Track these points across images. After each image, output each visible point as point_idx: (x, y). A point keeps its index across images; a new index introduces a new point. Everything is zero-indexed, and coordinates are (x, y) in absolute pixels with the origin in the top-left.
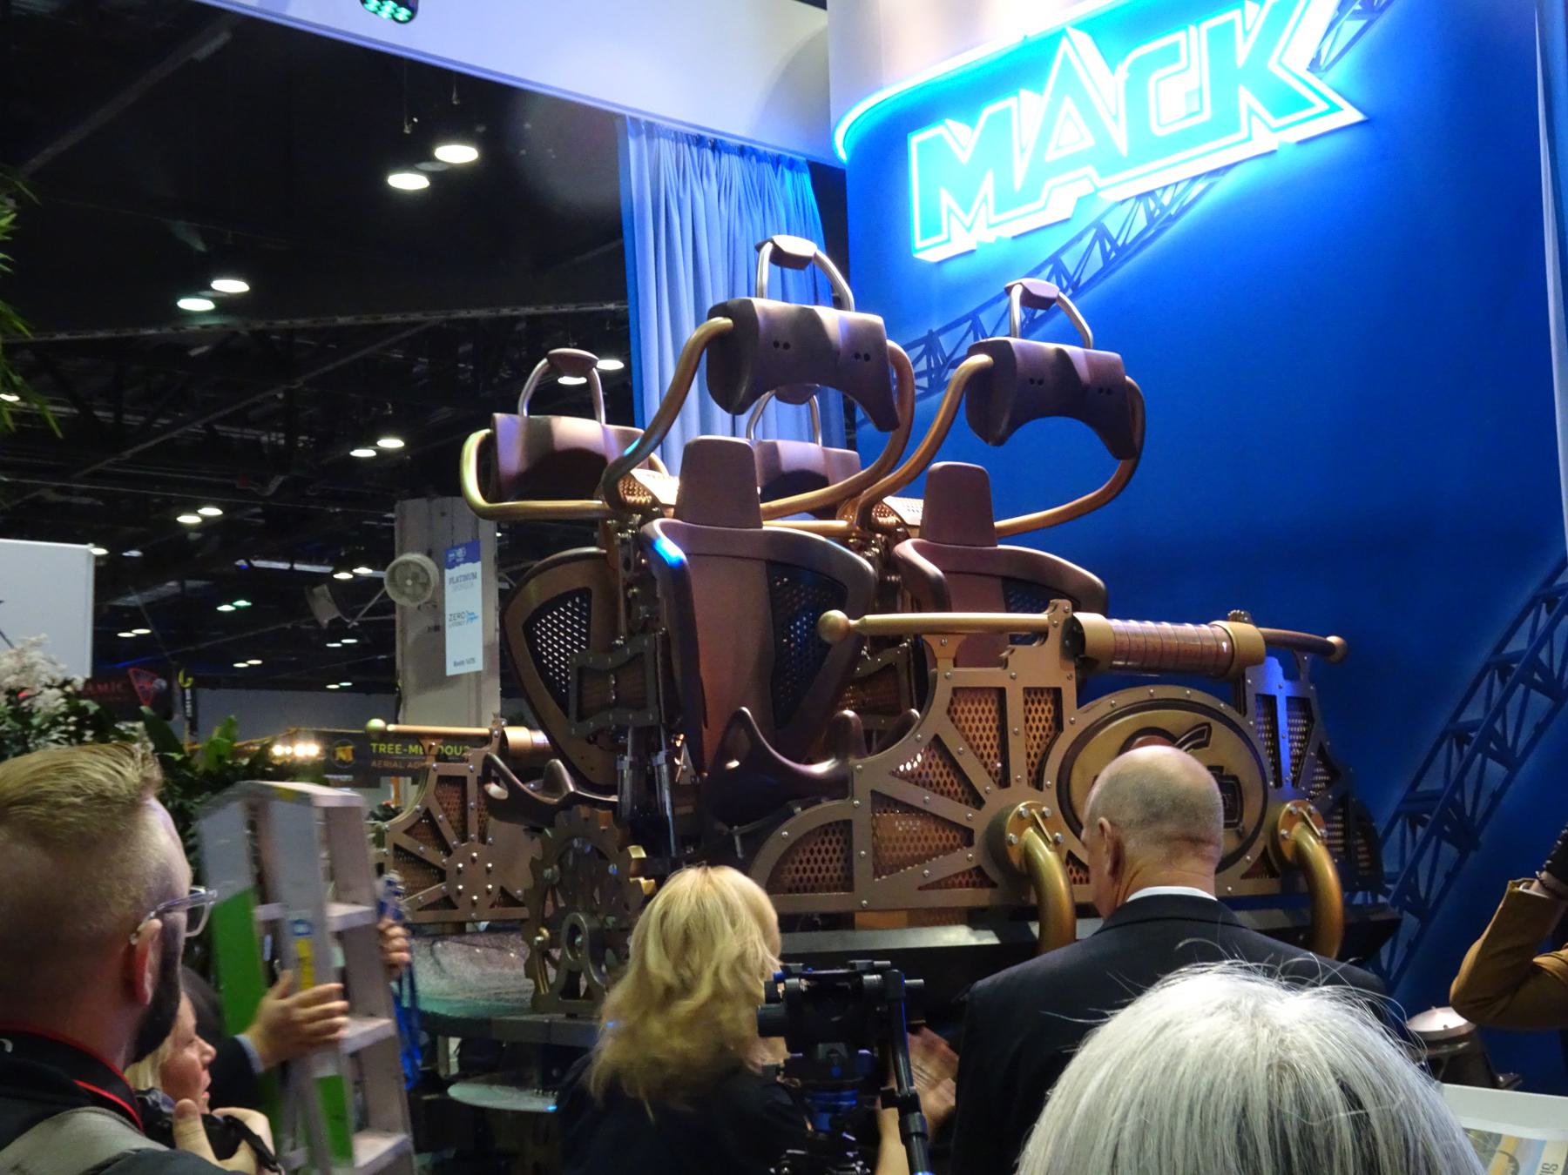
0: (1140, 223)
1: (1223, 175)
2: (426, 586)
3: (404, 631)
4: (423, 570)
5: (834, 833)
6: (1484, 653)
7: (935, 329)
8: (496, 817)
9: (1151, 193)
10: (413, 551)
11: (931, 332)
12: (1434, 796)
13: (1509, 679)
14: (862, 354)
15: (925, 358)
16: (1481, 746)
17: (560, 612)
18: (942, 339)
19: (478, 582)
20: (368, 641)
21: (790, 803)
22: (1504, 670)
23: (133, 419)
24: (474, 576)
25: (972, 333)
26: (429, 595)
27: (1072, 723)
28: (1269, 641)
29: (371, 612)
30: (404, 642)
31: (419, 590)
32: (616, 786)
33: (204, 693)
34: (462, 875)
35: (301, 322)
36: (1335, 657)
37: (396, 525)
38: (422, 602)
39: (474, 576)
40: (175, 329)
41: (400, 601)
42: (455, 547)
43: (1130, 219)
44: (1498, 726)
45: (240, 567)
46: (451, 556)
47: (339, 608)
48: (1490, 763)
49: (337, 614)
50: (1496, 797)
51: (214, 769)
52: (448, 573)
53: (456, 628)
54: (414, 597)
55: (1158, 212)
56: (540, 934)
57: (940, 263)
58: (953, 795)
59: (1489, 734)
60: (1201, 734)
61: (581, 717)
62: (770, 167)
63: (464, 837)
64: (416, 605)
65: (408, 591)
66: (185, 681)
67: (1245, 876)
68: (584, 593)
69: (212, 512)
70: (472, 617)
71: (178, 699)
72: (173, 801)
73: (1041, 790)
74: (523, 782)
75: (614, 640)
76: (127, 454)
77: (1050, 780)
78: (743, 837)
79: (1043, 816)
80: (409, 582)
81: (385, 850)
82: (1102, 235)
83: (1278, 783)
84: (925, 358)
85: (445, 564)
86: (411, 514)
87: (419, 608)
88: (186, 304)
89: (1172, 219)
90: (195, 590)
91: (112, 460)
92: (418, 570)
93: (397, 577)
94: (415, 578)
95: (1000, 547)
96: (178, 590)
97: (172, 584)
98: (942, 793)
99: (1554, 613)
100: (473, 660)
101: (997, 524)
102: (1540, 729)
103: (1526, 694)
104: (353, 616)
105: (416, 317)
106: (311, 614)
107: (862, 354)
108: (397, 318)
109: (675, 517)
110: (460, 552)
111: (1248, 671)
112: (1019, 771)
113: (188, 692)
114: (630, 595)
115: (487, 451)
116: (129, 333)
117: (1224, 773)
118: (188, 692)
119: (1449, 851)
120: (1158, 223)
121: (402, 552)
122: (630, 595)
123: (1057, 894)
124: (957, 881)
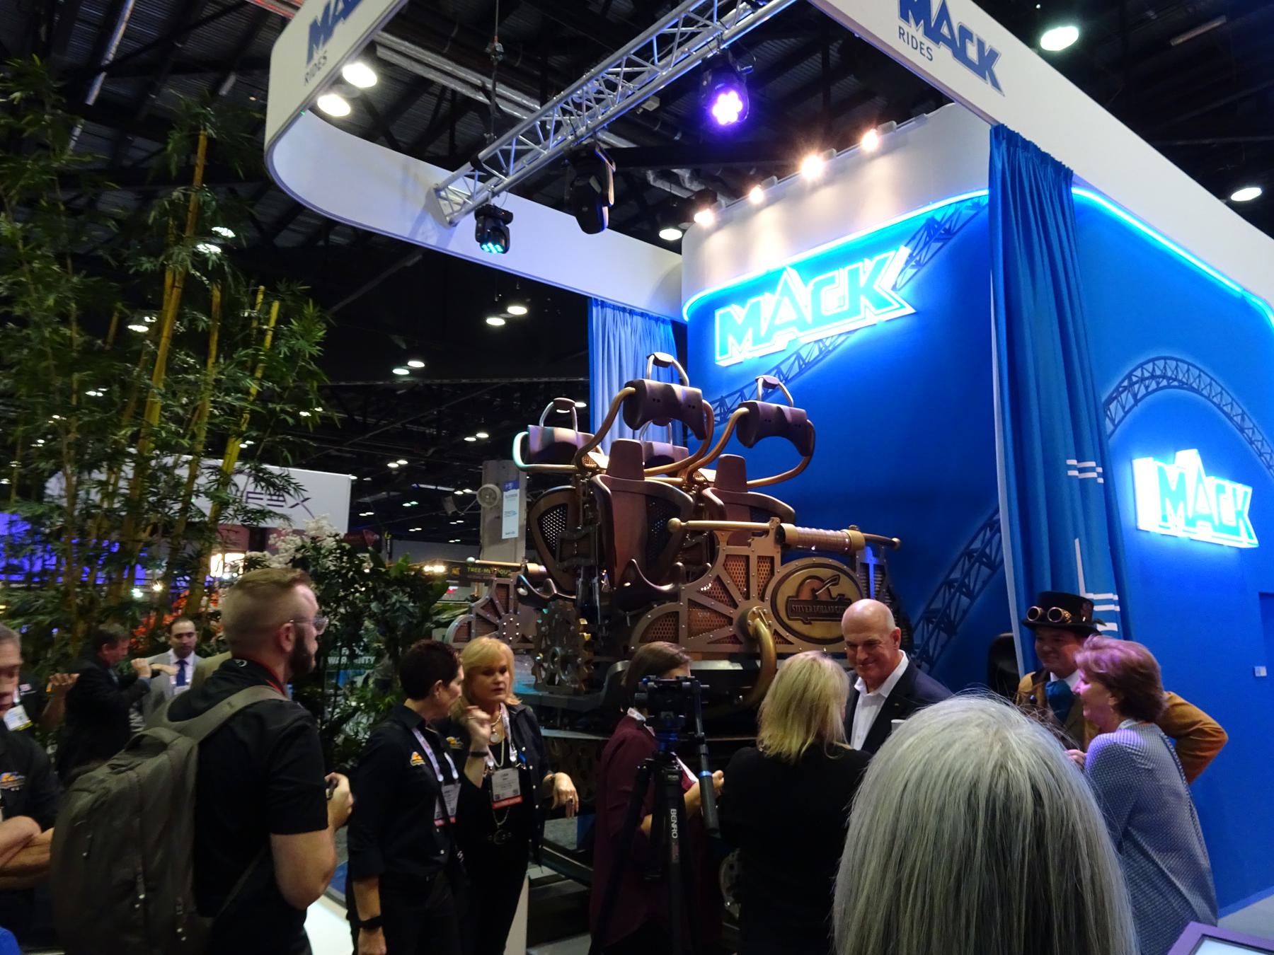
0: (816, 353)
2: (495, 499)
3: (484, 517)
4: (494, 492)
6: (962, 548)
7: (724, 395)
10: (490, 483)
18: (727, 400)
23: (371, 420)
24: (516, 495)
31: (492, 500)
33: (395, 542)
37: (483, 471)
39: (516, 495)
41: (483, 505)
54: (489, 503)
59: (962, 584)
60: (835, 580)
61: (561, 560)
70: (515, 513)
71: (384, 544)
76: (367, 436)
77: (768, 597)
79: (764, 613)
82: (799, 357)
85: (504, 489)
89: (830, 352)
90: (394, 496)
94: (490, 495)
97: (384, 493)
101: (748, 482)
103: (979, 567)
104: (462, 510)
106: (444, 509)
108: (488, 381)
109: (606, 474)
110: (510, 485)
112: (754, 593)
115: (525, 441)
116: (371, 383)
119: (943, 636)
120: (824, 353)
121: (485, 483)
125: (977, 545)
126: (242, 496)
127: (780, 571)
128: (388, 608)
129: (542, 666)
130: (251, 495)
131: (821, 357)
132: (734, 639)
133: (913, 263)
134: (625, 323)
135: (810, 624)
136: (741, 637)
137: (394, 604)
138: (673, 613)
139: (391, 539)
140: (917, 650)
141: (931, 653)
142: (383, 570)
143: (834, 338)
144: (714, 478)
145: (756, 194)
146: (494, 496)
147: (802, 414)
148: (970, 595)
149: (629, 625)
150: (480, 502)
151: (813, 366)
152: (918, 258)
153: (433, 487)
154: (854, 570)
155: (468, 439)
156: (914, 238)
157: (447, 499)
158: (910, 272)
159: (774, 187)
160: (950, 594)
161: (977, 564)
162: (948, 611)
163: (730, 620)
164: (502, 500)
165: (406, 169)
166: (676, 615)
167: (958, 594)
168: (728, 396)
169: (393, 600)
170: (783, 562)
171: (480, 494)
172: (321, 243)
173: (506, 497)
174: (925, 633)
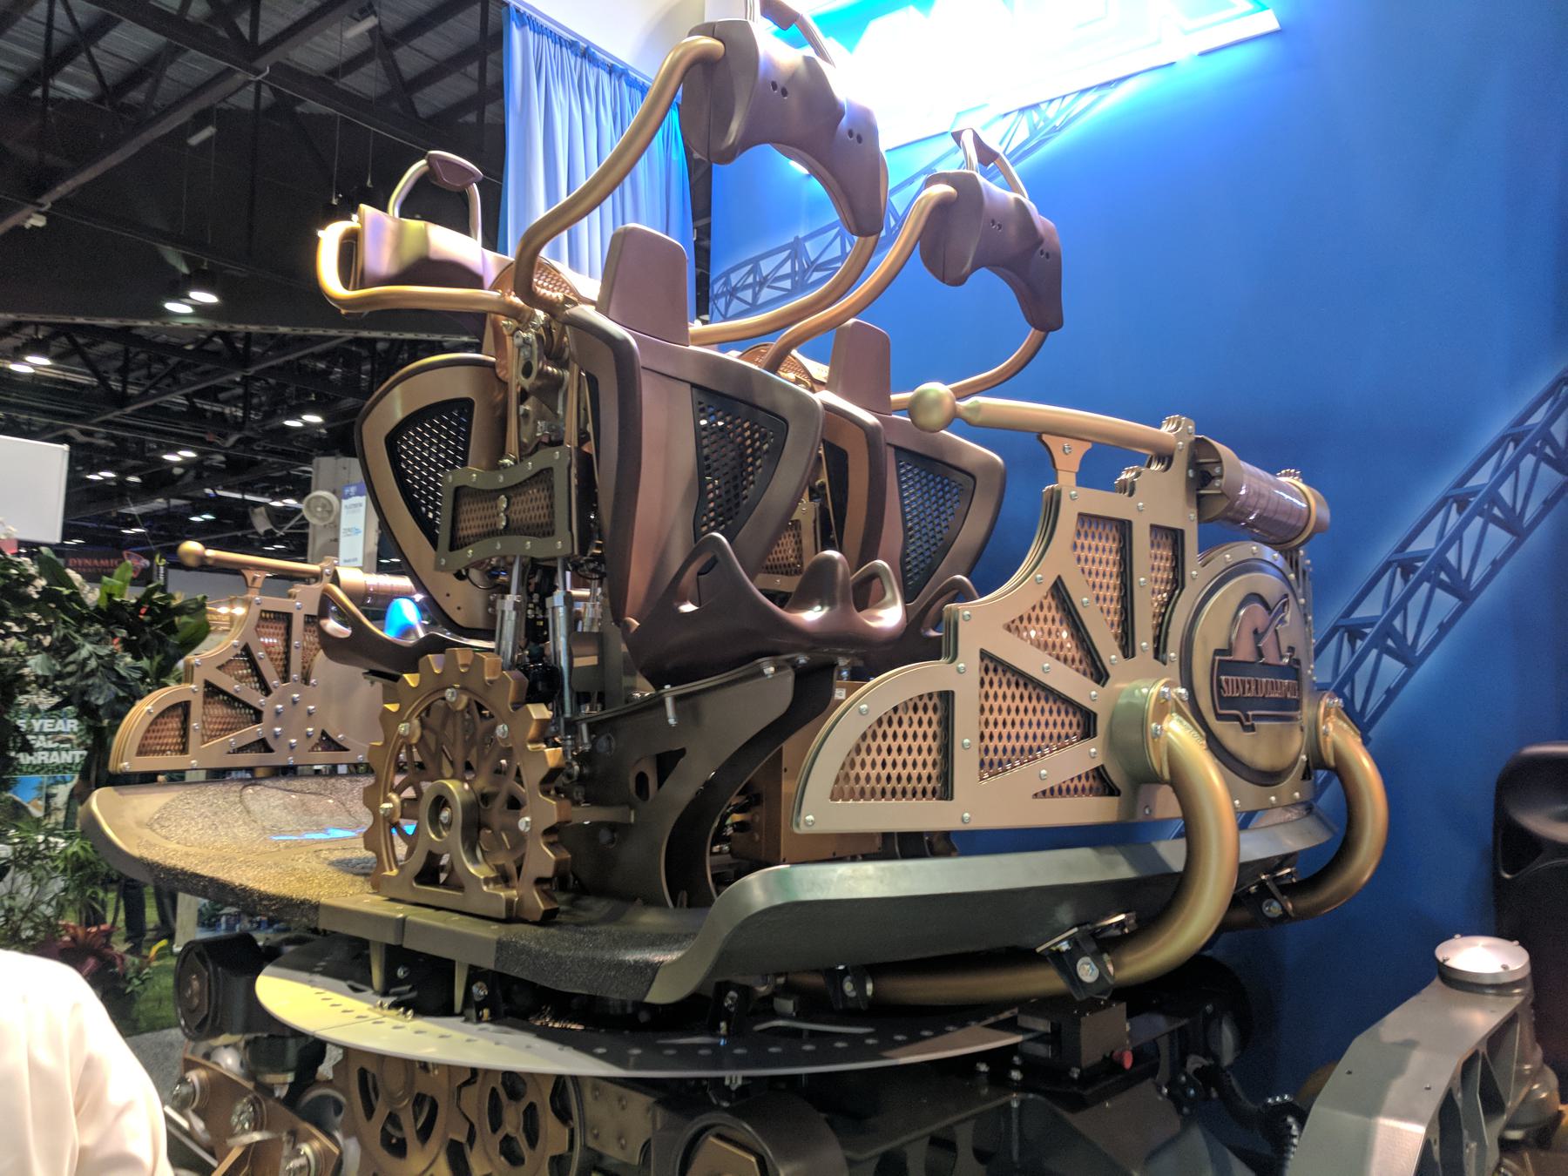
0: (1022, 135)
1: (1116, 86)
2: (330, 512)
3: (314, 539)
4: (330, 503)
5: (925, 709)
6: (1385, 550)
7: (801, 235)
8: (327, 653)
9: (1036, 106)
10: (323, 489)
11: (797, 238)
13: (1413, 577)
15: (789, 263)
16: (1378, 642)
17: (433, 424)
18: (808, 245)
19: (363, 509)
20: (292, 548)
21: (760, 660)
22: (1407, 568)
23: (133, 390)
24: (361, 505)
25: (839, 239)
26: (332, 519)
29: (291, 528)
30: (313, 548)
31: (326, 515)
32: (494, 631)
33: (172, 572)
34: (313, 716)
35: (254, 328)
37: (313, 476)
38: (326, 523)
39: (361, 505)
40: (164, 324)
41: (312, 520)
42: (349, 485)
43: (1011, 134)
44: (1397, 623)
45: (207, 495)
46: (347, 491)
47: (272, 523)
48: (1386, 659)
49: (269, 527)
50: (1391, 694)
51: (104, 605)
52: (345, 502)
53: (348, 538)
54: (322, 519)
55: (1042, 124)
56: (387, 800)
58: (1070, 662)
59: (1387, 630)
61: (455, 544)
63: (285, 678)
64: (322, 524)
65: (318, 515)
66: (160, 561)
68: (465, 405)
69: (190, 454)
70: (357, 531)
71: (155, 573)
72: (58, 631)
74: (108, 15)
75: (501, 458)
76: (129, 410)
78: (677, 699)
80: (319, 509)
81: (193, 686)
84: (789, 263)
85: (342, 496)
86: (324, 467)
87: (325, 526)
88: (171, 306)
90: (176, 507)
91: (118, 413)
92: (325, 502)
93: (312, 505)
94: (324, 506)
95: (894, 416)
96: (165, 506)
97: (161, 500)
99: (1465, 514)
100: (355, 560)
101: (894, 397)
102: (1444, 628)
103: (1431, 592)
104: (281, 529)
105: (333, 332)
106: (253, 527)
108: (320, 332)
110: (353, 489)
113: (162, 568)
114: (521, 412)
116: (129, 323)
118: (162, 568)
121: (317, 489)
122: (521, 412)
125: (1425, 542)
128: (70, 668)
129: (396, 825)
131: (1033, 143)
132: (1101, 783)
135: (1252, 728)
137: (86, 660)
139: (167, 567)
142: (66, 592)
143: (1068, 99)
144: (826, 375)
146: (328, 508)
148: (1411, 661)
149: (672, 721)
150: (308, 517)
153: (238, 496)
155: (289, 423)
157: (257, 510)
160: (1353, 652)
161: (1426, 586)
163: (1087, 723)
164: (339, 515)
167: (1374, 652)
168: (807, 238)
169: (84, 653)
171: (308, 506)
172: (38, 92)
173: (346, 507)
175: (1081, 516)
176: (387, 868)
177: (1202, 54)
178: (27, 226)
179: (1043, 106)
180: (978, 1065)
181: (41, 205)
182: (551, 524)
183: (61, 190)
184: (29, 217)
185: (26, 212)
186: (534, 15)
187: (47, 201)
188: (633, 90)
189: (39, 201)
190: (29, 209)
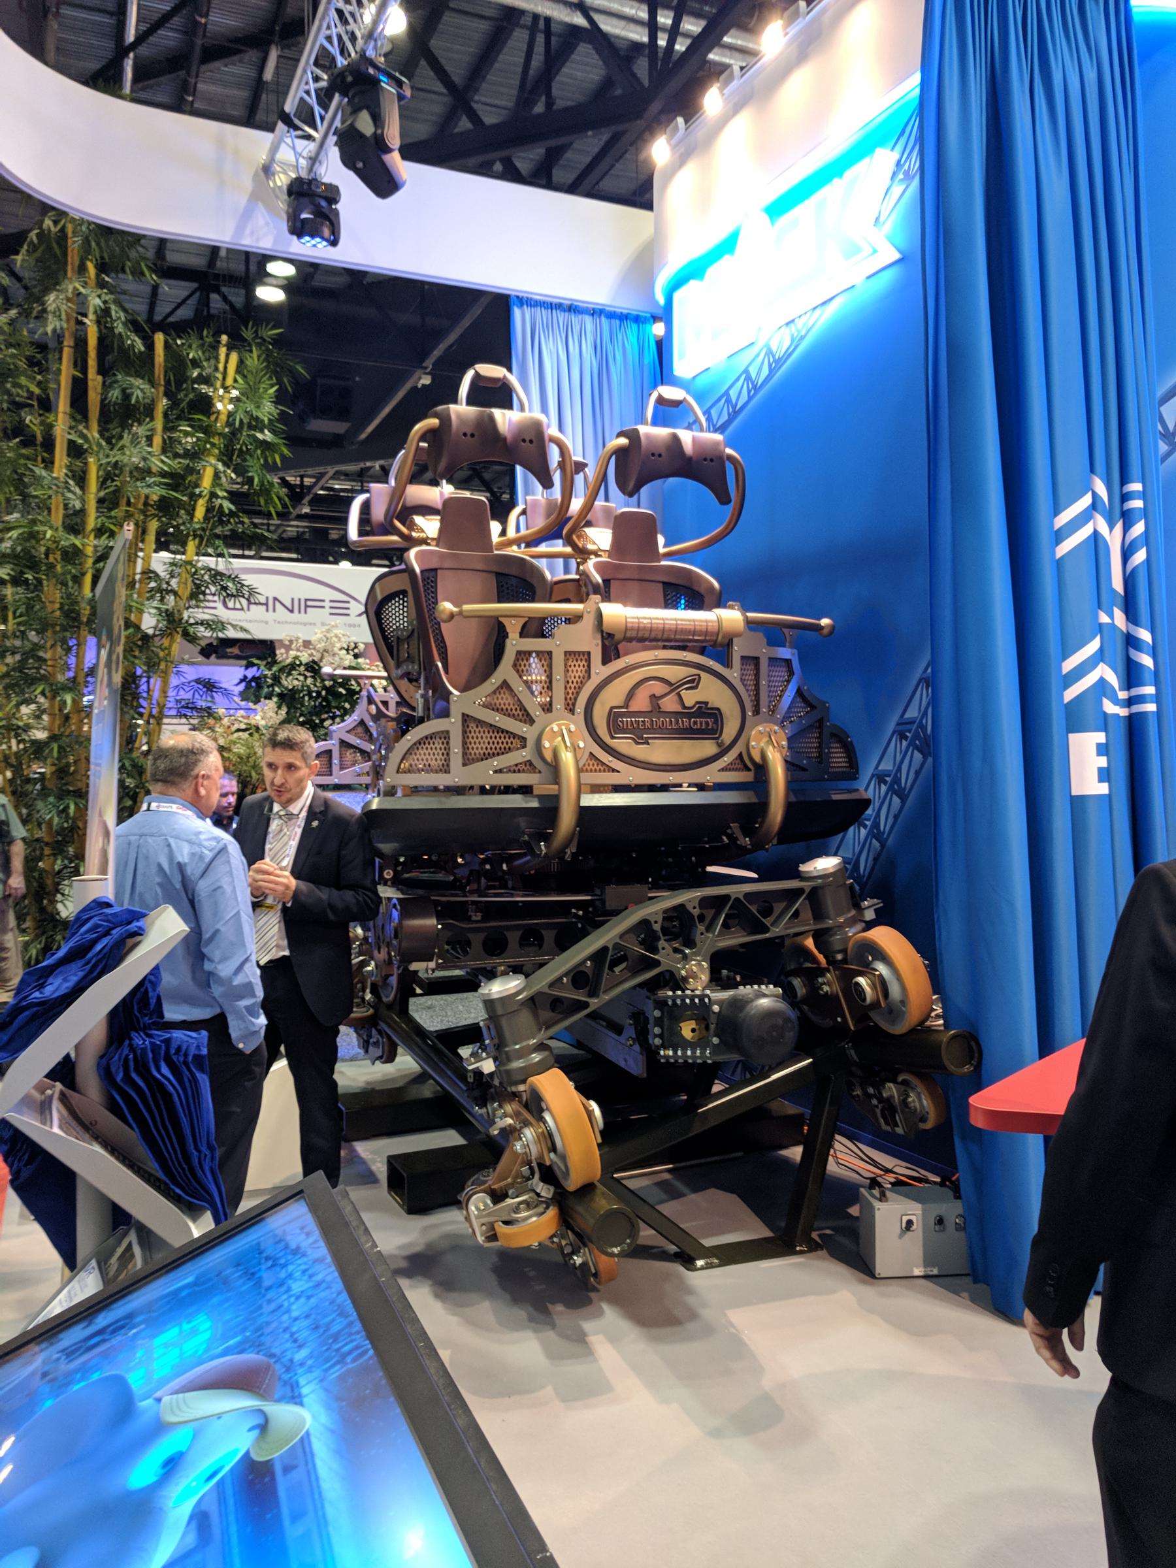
9: (793, 321)
12: (911, 722)
14: (528, 440)
27: (597, 674)
28: (750, 624)
36: (826, 631)
57: (694, 378)
60: (692, 681)
62: (618, 322)
67: (722, 770)
73: (573, 714)
77: (580, 708)
79: (569, 731)
82: (770, 352)
83: (757, 711)
89: (802, 338)
98: (509, 716)
107: (528, 440)
109: (437, 545)
111: (735, 640)
112: (559, 705)
115: (366, 508)
117: (709, 706)
119: (918, 756)
120: (796, 341)
123: (568, 780)
124: (516, 769)
126: (208, 601)
127: (600, 671)
130: (309, 603)
133: (901, 176)
134: (549, 327)
136: (538, 763)
138: (442, 732)
140: (888, 779)
141: (903, 785)
145: (713, 100)
147: (717, 443)
151: (785, 362)
152: (906, 167)
154: (727, 664)
156: (902, 133)
158: (898, 189)
159: (735, 84)
162: (924, 721)
165: (220, 143)
166: (445, 735)
170: (606, 660)
174: (898, 754)
175: (566, 653)
176: (730, 1072)
177: (869, 277)
178: (419, 386)
179: (796, 321)
180: (352, 924)
181: (426, 368)
182: (566, 660)
183: (437, 353)
184: (420, 378)
185: (416, 376)
186: (530, 296)
187: (429, 363)
188: (613, 321)
189: (424, 365)
190: (419, 372)
